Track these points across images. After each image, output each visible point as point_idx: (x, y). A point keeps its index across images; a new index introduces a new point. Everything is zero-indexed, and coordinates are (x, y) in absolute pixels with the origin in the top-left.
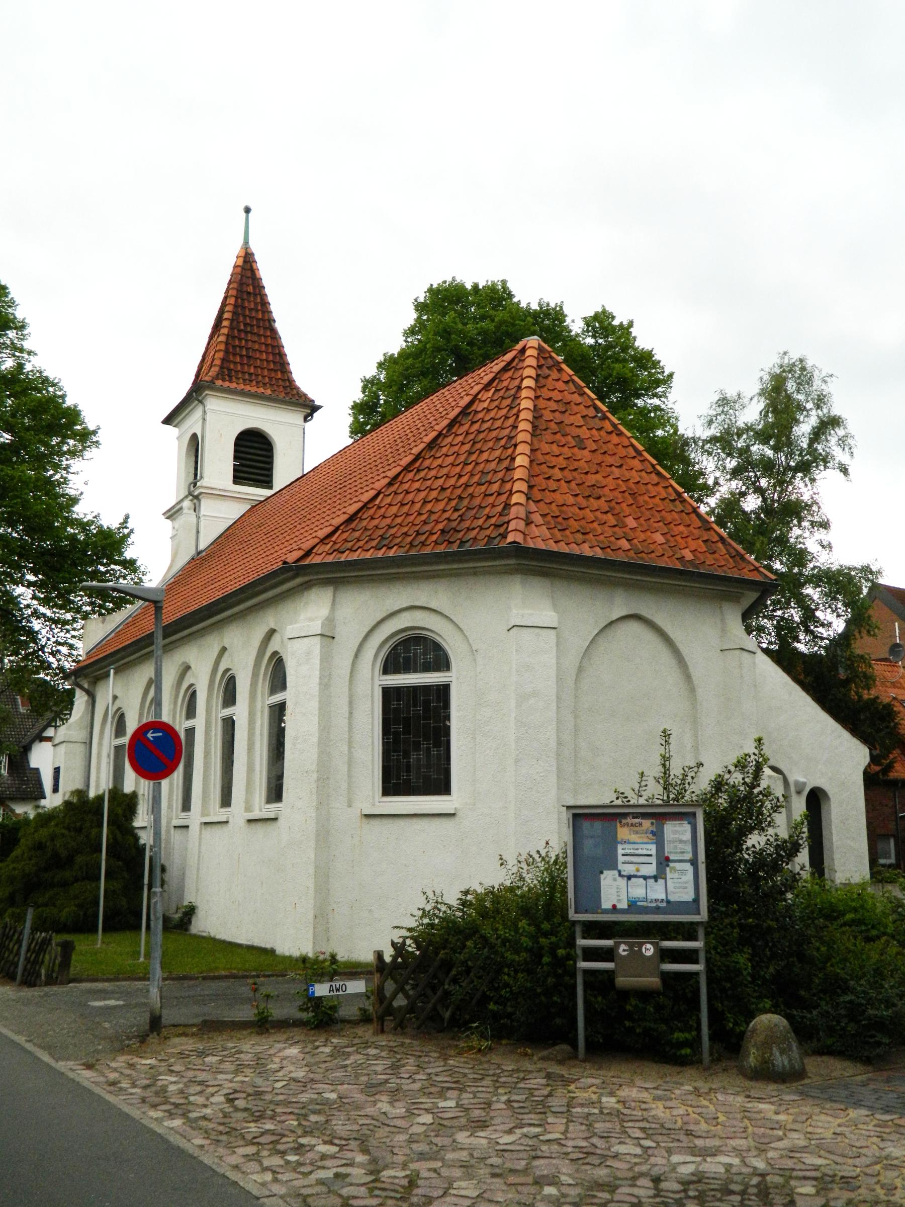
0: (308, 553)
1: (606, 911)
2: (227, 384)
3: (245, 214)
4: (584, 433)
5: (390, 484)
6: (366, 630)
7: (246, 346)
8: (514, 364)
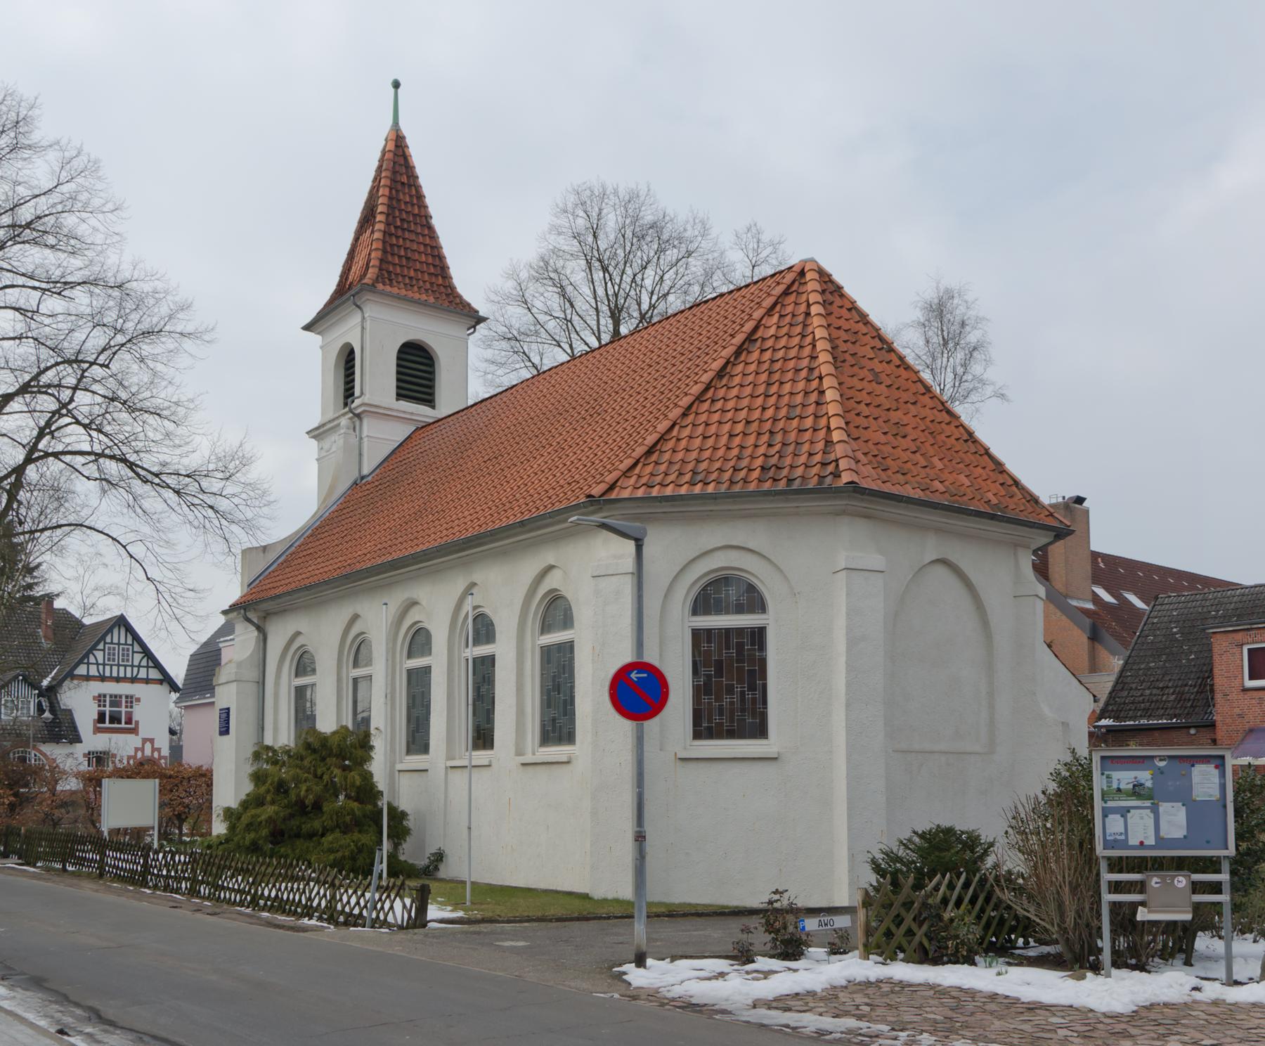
0: (612, 487)
1: (1133, 848)
2: (388, 288)
3: (393, 90)
4: (878, 367)
5: (684, 415)
6: (678, 569)
7: (398, 243)
8: (794, 288)
